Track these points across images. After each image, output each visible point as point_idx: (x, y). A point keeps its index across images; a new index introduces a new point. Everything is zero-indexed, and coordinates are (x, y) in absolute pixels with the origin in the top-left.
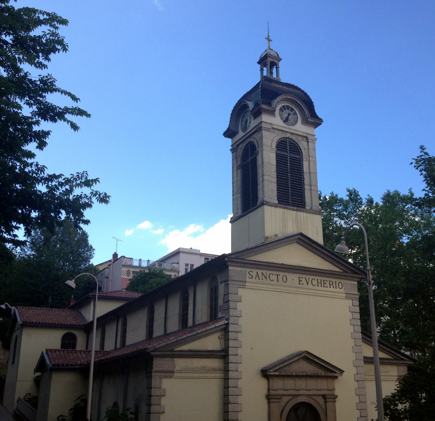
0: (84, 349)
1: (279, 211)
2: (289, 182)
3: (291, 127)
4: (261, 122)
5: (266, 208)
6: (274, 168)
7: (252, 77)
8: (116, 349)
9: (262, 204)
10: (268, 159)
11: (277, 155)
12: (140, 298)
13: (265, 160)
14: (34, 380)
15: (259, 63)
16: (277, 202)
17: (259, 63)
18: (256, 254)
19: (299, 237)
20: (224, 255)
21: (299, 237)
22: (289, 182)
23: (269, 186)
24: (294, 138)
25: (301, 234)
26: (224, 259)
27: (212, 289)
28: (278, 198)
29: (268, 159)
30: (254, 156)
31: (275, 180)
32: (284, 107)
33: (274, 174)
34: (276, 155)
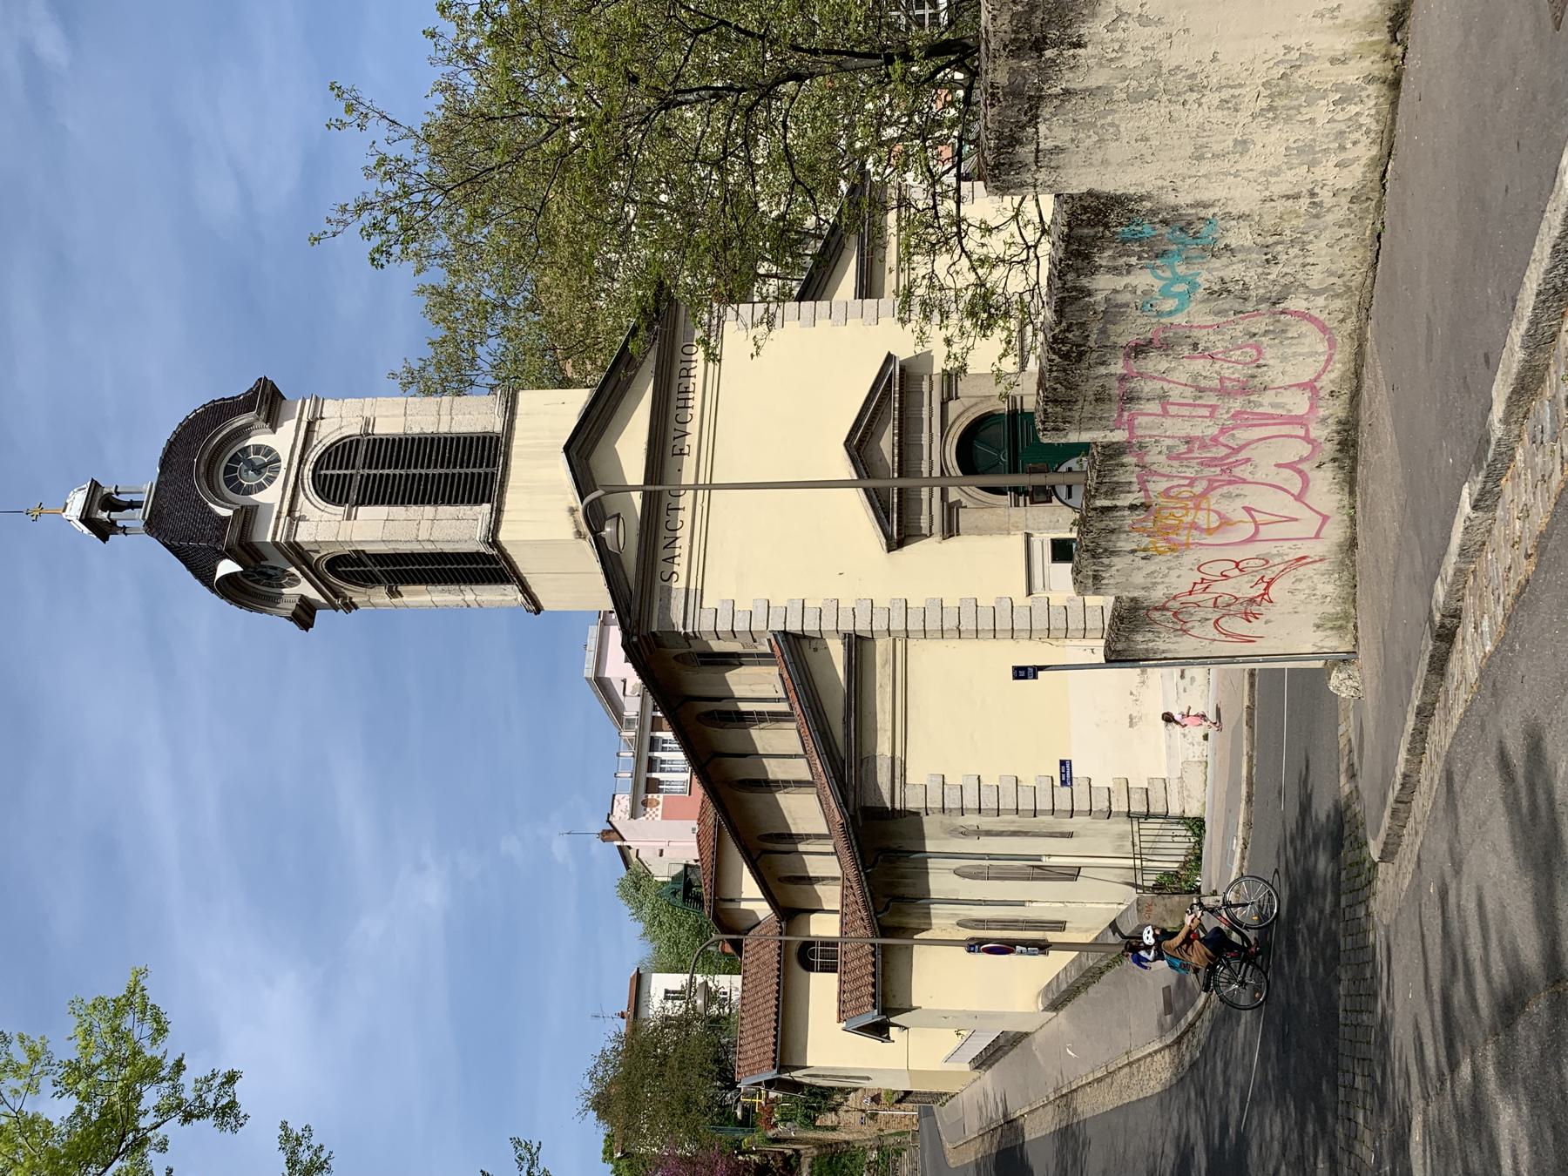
0: (838, 917)
1: (513, 499)
2: (431, 471)
3: (284, 464)
4: (276, 544)
5: (503, 537)
6: (398, 511)
7: (141, 552)
8: (835, 853)
9: (495, 544)
10: (378, 527)
11: (360, 502)
12: (687, 743)
13: (378, 536)
14: (1506, 999)
15: (104, 538)
16: (486, 507)
17: (104, 538)
18: (621, 566)
19: (573, 453)
20: (623, 646)
21: (573, 453)
22: (431, 471)
23: (452, 527)
24: (313, 456)
25: (567, 449)
26: (635, 645)
27: (704, 663)
28: (476, 503)
29: (378, 527)
30: (365, 559)
31: (429, 510)
32: (228, 482)
33: (414, 511)
34: (363, 504)
